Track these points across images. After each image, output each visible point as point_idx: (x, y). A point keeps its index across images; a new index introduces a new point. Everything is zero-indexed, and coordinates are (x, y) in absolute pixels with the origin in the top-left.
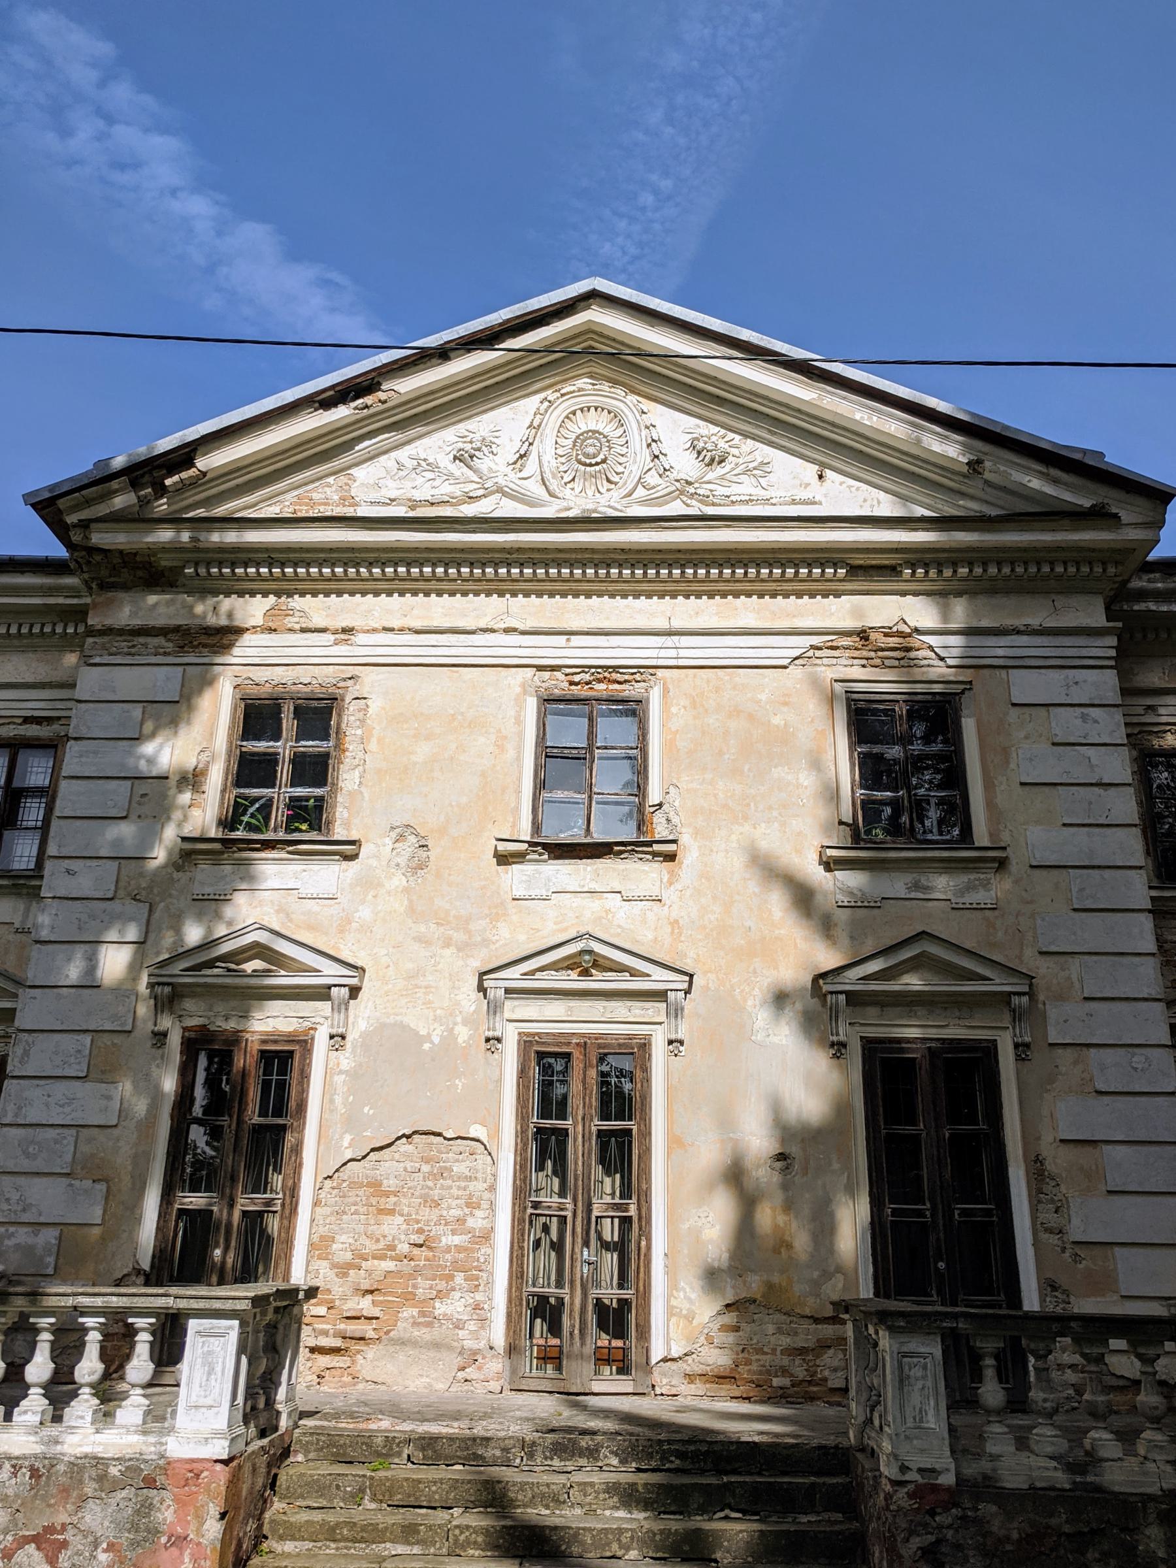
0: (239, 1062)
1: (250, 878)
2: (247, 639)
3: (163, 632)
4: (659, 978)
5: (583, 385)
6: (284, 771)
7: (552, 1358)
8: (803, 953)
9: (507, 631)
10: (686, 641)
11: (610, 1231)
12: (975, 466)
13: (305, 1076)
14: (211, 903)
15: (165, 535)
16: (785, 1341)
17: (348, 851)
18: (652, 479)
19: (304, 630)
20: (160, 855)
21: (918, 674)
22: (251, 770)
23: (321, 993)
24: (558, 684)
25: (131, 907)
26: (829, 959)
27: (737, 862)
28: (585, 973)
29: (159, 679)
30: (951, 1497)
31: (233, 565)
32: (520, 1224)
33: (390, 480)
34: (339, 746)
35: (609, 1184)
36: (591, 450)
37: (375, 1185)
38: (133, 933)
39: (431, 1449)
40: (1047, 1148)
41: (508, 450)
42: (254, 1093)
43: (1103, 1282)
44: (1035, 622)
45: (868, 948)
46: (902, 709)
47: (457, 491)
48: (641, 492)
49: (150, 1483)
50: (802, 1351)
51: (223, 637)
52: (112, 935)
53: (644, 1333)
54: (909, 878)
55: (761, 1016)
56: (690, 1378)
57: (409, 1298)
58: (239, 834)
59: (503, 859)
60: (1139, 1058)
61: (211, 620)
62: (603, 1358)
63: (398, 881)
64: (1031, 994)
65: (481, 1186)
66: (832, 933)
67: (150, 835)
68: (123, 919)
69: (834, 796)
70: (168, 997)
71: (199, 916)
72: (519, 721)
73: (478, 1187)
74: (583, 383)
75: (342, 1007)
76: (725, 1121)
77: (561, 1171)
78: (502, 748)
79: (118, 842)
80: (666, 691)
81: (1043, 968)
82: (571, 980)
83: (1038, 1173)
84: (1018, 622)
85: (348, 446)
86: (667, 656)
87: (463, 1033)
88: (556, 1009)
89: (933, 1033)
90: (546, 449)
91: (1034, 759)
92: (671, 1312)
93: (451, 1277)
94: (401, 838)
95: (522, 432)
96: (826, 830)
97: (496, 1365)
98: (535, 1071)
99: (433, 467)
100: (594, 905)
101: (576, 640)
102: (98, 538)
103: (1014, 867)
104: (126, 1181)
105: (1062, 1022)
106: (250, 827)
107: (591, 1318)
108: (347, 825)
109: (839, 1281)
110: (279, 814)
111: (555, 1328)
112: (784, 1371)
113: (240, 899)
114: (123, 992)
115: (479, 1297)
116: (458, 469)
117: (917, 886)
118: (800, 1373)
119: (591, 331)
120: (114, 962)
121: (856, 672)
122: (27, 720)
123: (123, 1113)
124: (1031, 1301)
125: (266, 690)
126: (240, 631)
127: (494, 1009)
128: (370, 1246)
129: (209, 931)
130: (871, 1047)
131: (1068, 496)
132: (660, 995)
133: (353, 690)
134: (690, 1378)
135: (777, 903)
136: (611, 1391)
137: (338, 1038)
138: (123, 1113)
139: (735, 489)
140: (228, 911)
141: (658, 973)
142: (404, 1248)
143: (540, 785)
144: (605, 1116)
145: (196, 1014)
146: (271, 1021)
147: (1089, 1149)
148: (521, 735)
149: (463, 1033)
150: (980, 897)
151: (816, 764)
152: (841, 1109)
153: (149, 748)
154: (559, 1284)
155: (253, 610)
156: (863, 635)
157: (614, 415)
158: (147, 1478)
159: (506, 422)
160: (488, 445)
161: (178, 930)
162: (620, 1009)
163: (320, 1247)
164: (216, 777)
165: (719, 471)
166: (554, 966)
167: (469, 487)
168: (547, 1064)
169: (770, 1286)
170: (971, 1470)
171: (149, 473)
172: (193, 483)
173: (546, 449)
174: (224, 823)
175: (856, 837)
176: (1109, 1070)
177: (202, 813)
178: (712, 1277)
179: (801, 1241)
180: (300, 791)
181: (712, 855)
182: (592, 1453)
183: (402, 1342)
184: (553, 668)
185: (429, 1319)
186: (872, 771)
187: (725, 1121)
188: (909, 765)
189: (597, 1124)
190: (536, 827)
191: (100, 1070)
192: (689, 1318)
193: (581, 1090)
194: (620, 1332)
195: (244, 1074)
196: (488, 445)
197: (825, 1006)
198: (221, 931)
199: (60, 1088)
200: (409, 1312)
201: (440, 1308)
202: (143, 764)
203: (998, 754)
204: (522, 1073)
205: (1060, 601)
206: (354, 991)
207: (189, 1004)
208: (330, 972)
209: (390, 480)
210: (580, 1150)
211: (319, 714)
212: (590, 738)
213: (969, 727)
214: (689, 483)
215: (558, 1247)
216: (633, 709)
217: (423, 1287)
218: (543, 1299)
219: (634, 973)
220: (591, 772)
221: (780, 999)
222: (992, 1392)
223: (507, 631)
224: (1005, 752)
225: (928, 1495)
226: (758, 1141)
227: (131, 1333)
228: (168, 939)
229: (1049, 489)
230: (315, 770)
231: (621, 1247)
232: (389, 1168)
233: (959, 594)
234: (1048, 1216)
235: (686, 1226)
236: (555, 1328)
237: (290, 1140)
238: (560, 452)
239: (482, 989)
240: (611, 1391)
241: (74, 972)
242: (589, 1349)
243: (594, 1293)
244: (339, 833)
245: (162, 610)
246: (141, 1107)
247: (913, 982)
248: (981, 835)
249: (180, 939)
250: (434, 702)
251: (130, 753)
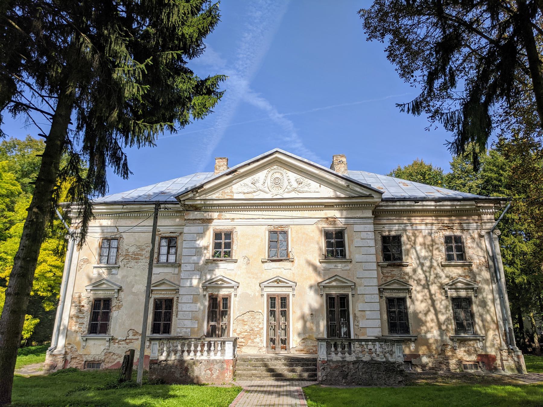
0: (219, 300)
1: (218, 266)
2: (215, 221)
3: (199, 219)
4: (291, 284)
6: (223, 246)
7: (274, 348)
8: (315, 279)
10: (295, 220)
11: (283, 327)
12: (348, 186)
13: (230, 302)
14: (211, 271)
15: (199, 202)
16: (312, 344)
17: (235, 261)
18: (289, 187)
20: (201, 262)
21: (337, 226)
22: (217, 246)
24: (272, 228)
25: (197, 272)
26: (320, 280)
27: (304, 262)
28: (278, 283)
29: (199, 229)
30: (326, 362)
31: (212, 207)
32: (268, 326)
33: (239, 190)
34: (233, 241)
35: (283, 319)
37: (243, 320)
38: (198, 277)
39: (257, 360)
40: (356, 312)
41: (261, 182)
42: (221, 305)
43: (364, 334)
44: (358, 216)
45: (327, 277)
46: (334, 233)
47: (252, 190)
49: (223, 362)
50: (315, 346)
51: (210, 220)
52: (194, 277)
53: (289, 344)
54: (335, 264)
55: (308, 290)
56: (296, 351)
57: (250, 339)
58: (215, 258)
59: (263, 262)
60: (373, 296)
61: (207, 217)
62: (282, 348)
63: (244, 266)
64: (355, 285)
67: (200, 259)
68: (196, 274)
69: (320, 249)
70: (205, 288)
71: (209, 273)
72: (265, 236)
73: (260, 320)
74: (275, 167)
75: (236, 290)
76: (301, 308)
77: (274, 316)
78: (262, 241)
79: (194, 260)
81: (357, 281)
82: (275, 284)
83: (355, 316)
84: (355, 216)
85: (231, 182)
87: (257, 294)
88: (273, 289)
89: (337, 293)
90: (268, 181)
91: (357, 242)
92: (293, 340)
94: (245, 258)
95: (264, 178)
96: (320, 255)
97: (264, 349)
98: (270, 300)
99: (247, 185)
100: (279, 271)
102: (186, 203)
103: (353, 262)
104: (201, 321)
105: (360, 290)
106: (218, 257)
107: (280, 342)
108: (235, 256)
109: (321, 335)
110: (222, 254)
111: (274, 343)
112: (312, 349)
113: (216, 270)
114: (197, 287)
116: (252, 186)
117: (336, 266)
118: (315, 349)
119: (276, 157)
120: (195, 282)
121: (325, 226)
122: (171, 233)
123: (199, 309)
125: (219, 231)
126: (213, 219)
127: (262, 290)
128: (243, 331)
129: (211, 277)
130: (327, 295)
131: (365, 192)
132: (291, 287)
134: (296, 351)
135: (311, 269)
136: (283, 353)
137: (236, 295)
138: (199, 309)
139: (304, 189)
140: (214, 272)
141: (290, 283)
142: (248, 331)
143: (269, 248)
144: (282, 307)
145: (210, 291)
146: (223, 292)
148: (265, 238)
149: (257, 294)
150: (345, 268)
151: (318, 244)
152: (322, 306)
153: (198, 242)
154: (275, 336)
155: (215, 215)
156: (327, 218)
158: (222, 362)
159: (261, 175)
160: (257, 181)
161: (206, 276)
162: (284, 289)
163: (234, 331)
164: (211, 248)
165: (301, 185)
168: (272, 299)
169: (310, 336)
170: (329, 359)
171: (195, 190)
172: (203, 191)
173: (268, 181)
174: (213, 256)
175: (325, 257)
176: (367, 298)
177: (208, 254)
178: (299, 334)
179: (314, 328)
180: (226, 250)
181: (300, 260)
182: (280, 360)
183: (249, 346)
185: (253, 342)
186: (329, 244)
187: (301, 308)
188: (336, 244)
189: (280, 309)
190: (269, 256)
191: (195, 301)
192: (296, 341)
193: (278, 302)
194: (285, 344)
195: (220, 302)
196: (257, 181)
197: (319, 288)
198: (214, 277)
199: (188, 304)
200: (250, 341)
201: (255, 340)
202: (197, 246)
203: (351, 241)
204: (267, 301)
205: (364, 211)
206: (238, 287)
207: (209, 289)
208: (234, 284)
209: (239, 190)
210: (278, 313)
211: (229, 235)
212: (278, 241)
213: (346, 236)
215: (274, 330)
216: (285, 233)
217: (252, 337)
218: (272, 339)
219: (286, 283)
220: (278, 245)
221: (311, 287)
224: (352, 240)
225: (324, 362)
226: (307, 311)
227: (211, 344)
228: (204, 278)
229: (361, 191)
230: (228, 245)
231: (285, 330)
232: (245, 317)
233: (345, 210)
234: (356, 323)
235: (295, 326)
236: (274, 343)
237: (228, 312)
239: (260, 286)
240: (283, 353)
241: (188, 284)
242: (280, 346)
243: (280, 337)
245: (198, 215)
246: (202, 308)
247: (334, 284)
248: (347, 257)
249: (206, 278)
250: (250, 233)
251: (195, 243)
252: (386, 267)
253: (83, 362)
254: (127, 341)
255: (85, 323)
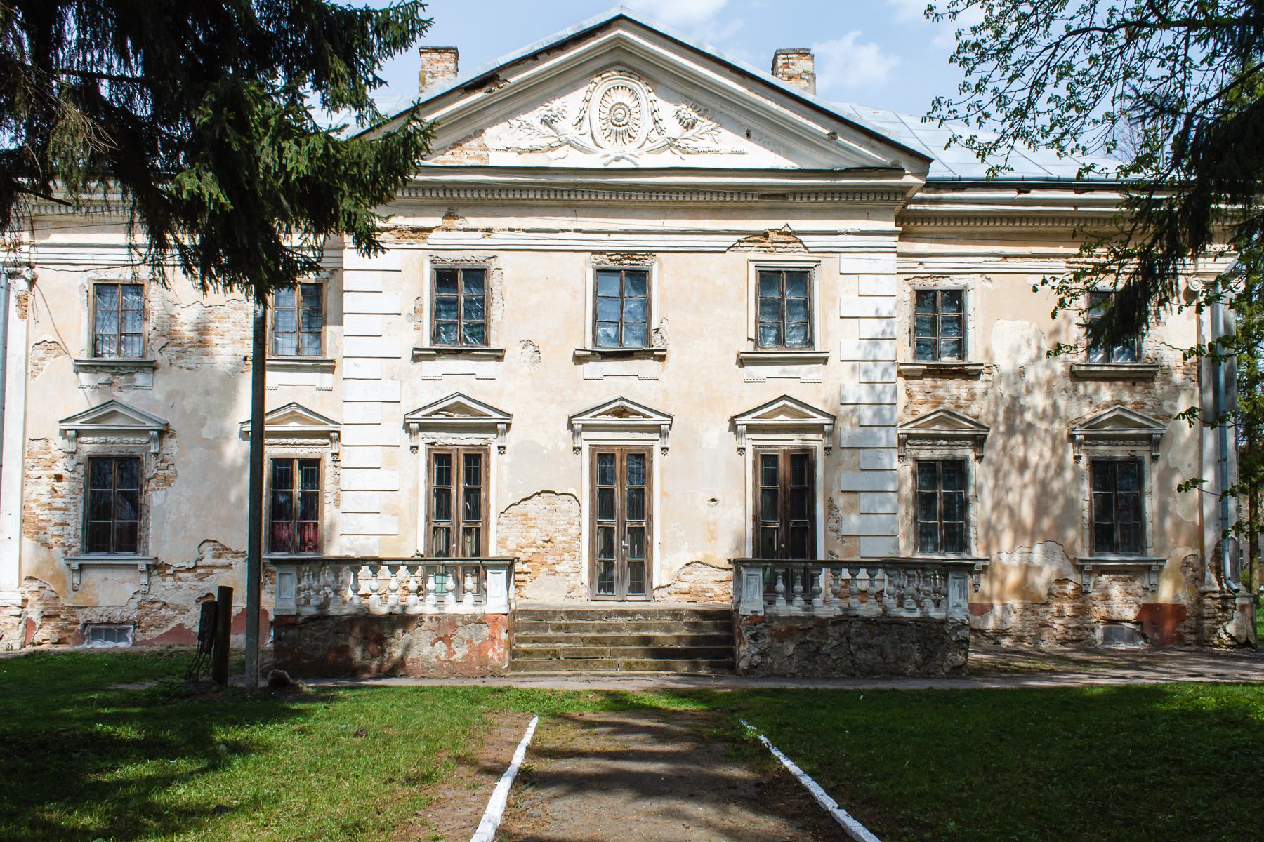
5: (613, 78)
9: (576, 231)
16: (713, 578)
17: (498, 356)
19: (465, 230)
23: (492, 428)
30: (762, 619)
36: (620, 117)
37: (525, 515)
40: (834, 494)
41: (572, 117)
48: (648, 145)
57: (543, 564)
65: (574, 515)
66: (1093, 350)
80: (661, 265)
83: (830, 506)
86: (661, 246)
92: (662, 567)
93: (562, 555)
97: (585, 590)
98: (597, 465)
101: (613, 237)
108: (497, 340)
115: (576, 562)
116: (545, 129)
124: (821, 556)
128: (524, 542)
133: (495, 264)
141: (656, 417)
147: (853, 495)
157: (633, 92)
159: (570, 103)
165: (691, 132)
166: (436, 413)
167: (551, 140)
168: (604, 460)
184: (601, 252)
189: (627, 486)
196: (561, 114)
200: (544, 569)
201: (558, 568)
206: (508, 425)
214: (675, 140)
217: (550, 559)
219: (645, 416)
222: (781, 586)
223: (576, 231)
225: (754, 620)
232: (530, 507)
238: (602, 116)
244: (493, 345)
252: (920, 378)
253: (79, 627)
254: (200, 571)
255: (72, 523)
